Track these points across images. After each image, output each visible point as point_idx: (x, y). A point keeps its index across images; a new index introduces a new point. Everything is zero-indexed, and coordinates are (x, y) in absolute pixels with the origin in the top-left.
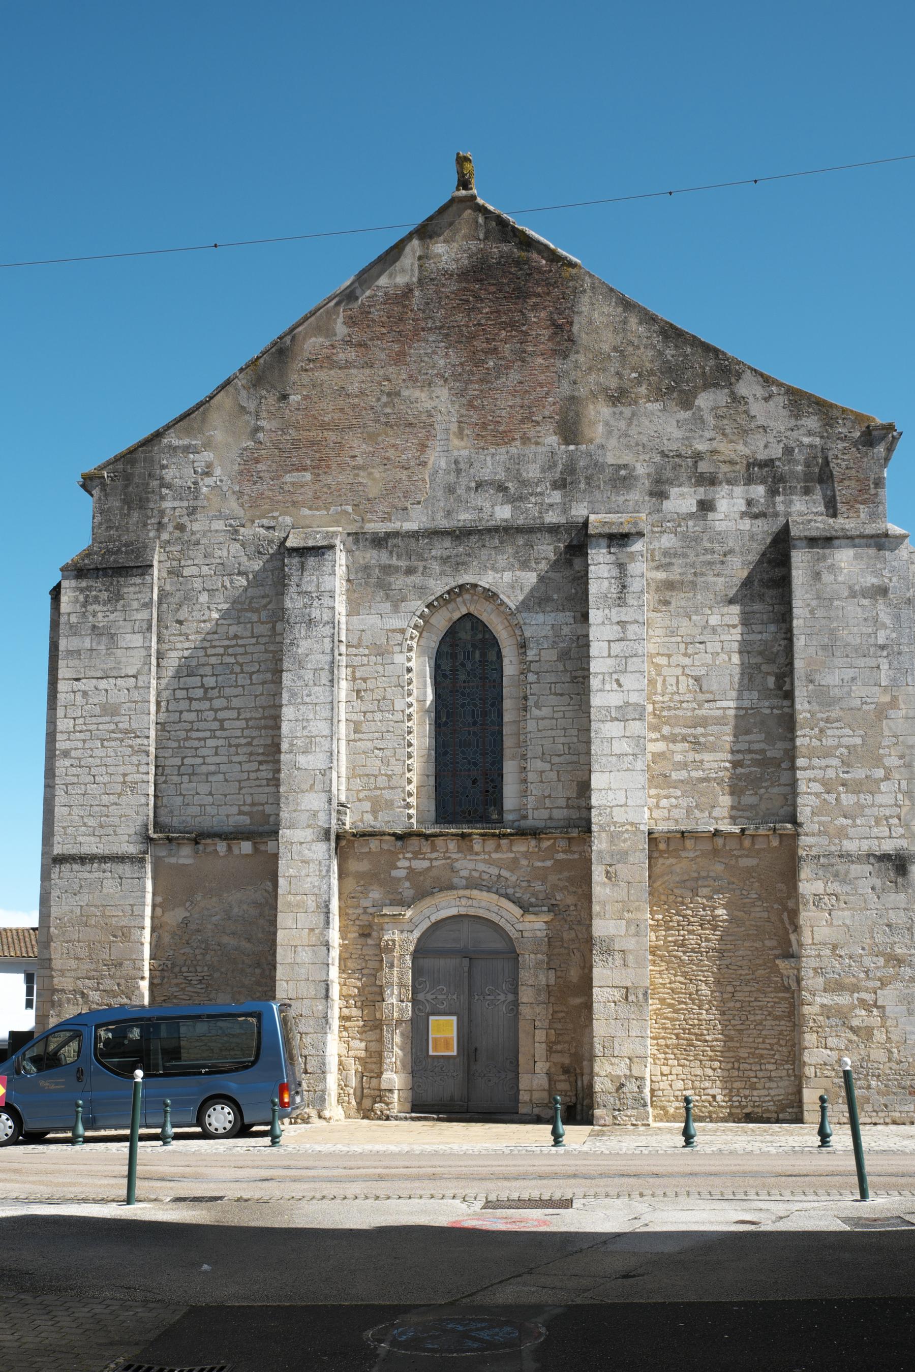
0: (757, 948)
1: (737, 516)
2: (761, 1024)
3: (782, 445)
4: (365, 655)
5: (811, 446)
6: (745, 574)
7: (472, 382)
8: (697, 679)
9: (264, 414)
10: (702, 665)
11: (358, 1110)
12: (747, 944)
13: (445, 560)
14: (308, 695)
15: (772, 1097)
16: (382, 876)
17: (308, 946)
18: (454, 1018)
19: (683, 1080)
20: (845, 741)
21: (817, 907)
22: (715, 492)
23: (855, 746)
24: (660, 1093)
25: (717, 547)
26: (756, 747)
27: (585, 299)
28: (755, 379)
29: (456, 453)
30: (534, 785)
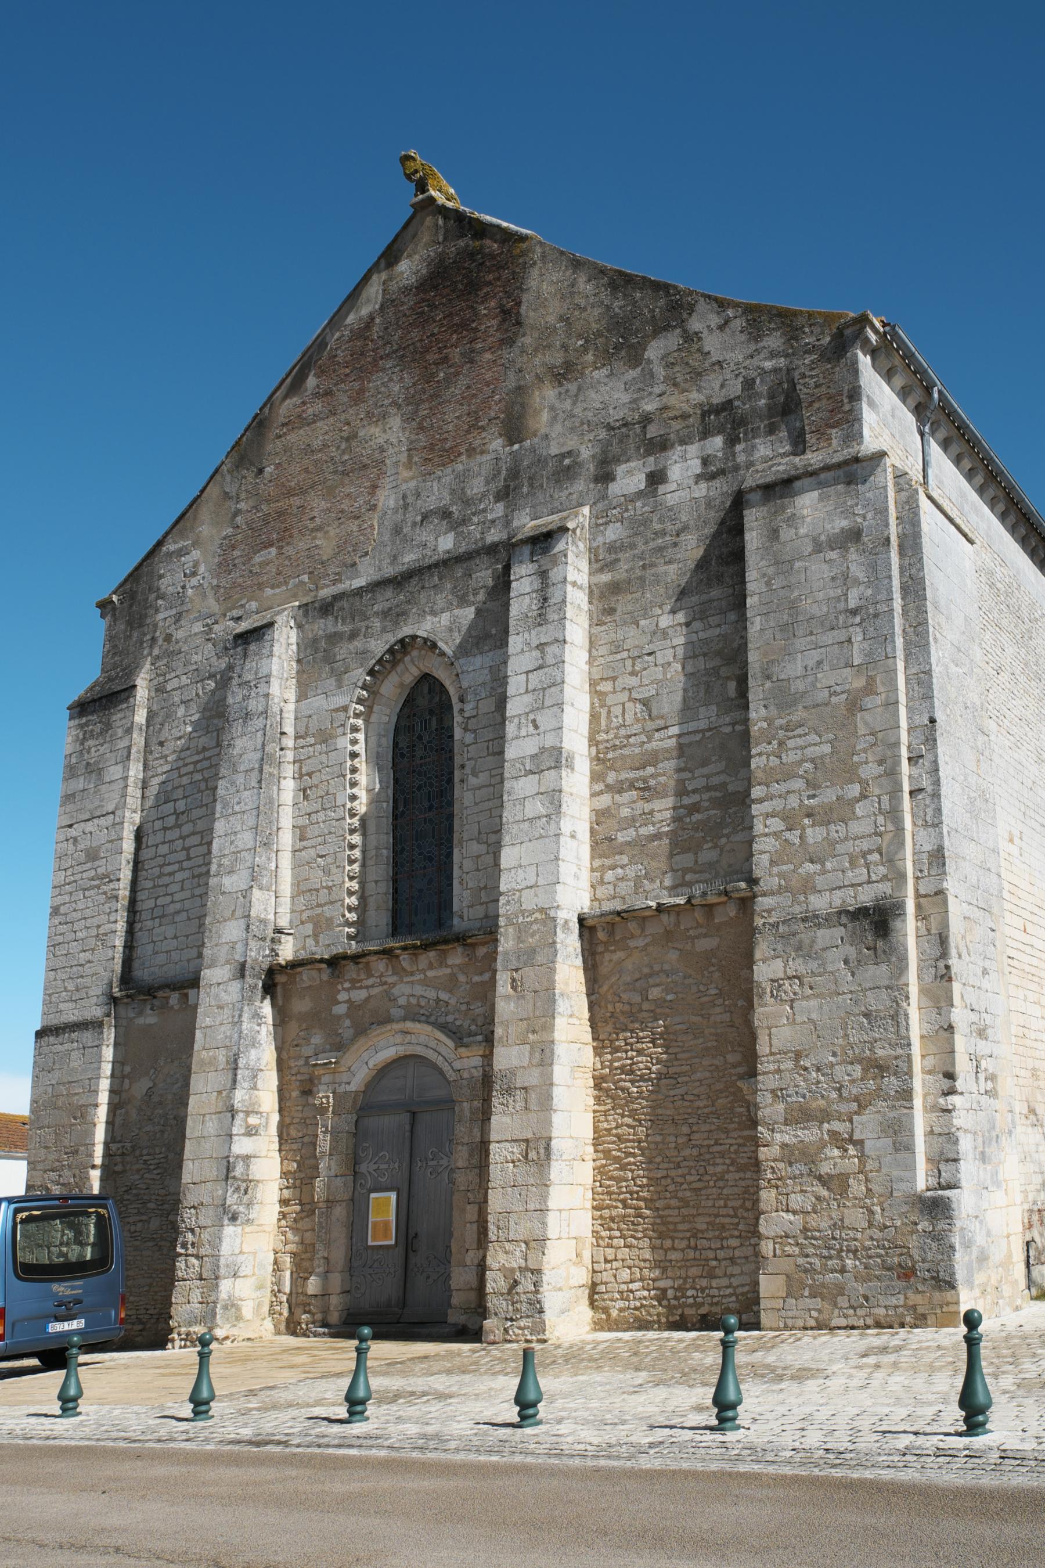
0: (717, 1067)
1: (691, 482)
2: (722, 1179)
3: (741, 379)
4: (311, 745)
5: (776, 370)
6: (700, 552)
7: (423, 401)
8: (646, 703)
9: (243, 496)
10: (652, 683)
11: (287, 1327)
12: (706, 1062)
13: (385, 614)
14: (238, 803)
15: (735, 1288)
16: (323, 1015)
17: (215, 1113)
18: (393, 1196)
19: (630, 1268)
21: (776, 998)
22: (666, 459)
23: (822, 757)
24: (602, 1288)
25: (669, 527)
26: (716, 780)
27: (535, 272)
28: (709, 307)
29: (404, 487)
30: (470, 875)
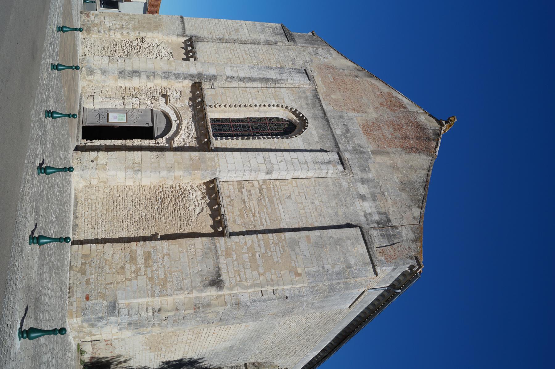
8: (289, 197)
20: (274, 254)
